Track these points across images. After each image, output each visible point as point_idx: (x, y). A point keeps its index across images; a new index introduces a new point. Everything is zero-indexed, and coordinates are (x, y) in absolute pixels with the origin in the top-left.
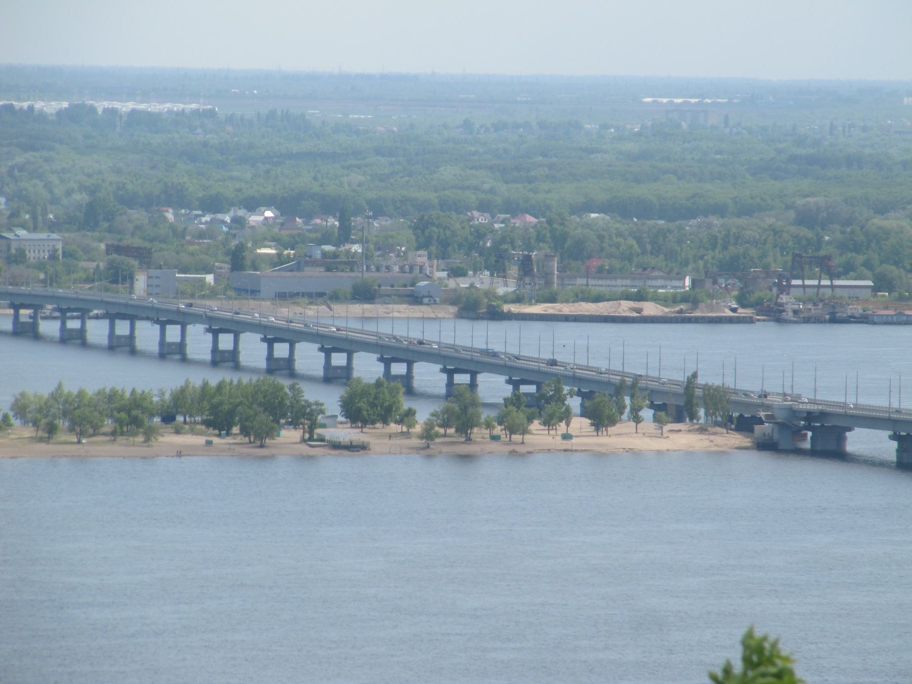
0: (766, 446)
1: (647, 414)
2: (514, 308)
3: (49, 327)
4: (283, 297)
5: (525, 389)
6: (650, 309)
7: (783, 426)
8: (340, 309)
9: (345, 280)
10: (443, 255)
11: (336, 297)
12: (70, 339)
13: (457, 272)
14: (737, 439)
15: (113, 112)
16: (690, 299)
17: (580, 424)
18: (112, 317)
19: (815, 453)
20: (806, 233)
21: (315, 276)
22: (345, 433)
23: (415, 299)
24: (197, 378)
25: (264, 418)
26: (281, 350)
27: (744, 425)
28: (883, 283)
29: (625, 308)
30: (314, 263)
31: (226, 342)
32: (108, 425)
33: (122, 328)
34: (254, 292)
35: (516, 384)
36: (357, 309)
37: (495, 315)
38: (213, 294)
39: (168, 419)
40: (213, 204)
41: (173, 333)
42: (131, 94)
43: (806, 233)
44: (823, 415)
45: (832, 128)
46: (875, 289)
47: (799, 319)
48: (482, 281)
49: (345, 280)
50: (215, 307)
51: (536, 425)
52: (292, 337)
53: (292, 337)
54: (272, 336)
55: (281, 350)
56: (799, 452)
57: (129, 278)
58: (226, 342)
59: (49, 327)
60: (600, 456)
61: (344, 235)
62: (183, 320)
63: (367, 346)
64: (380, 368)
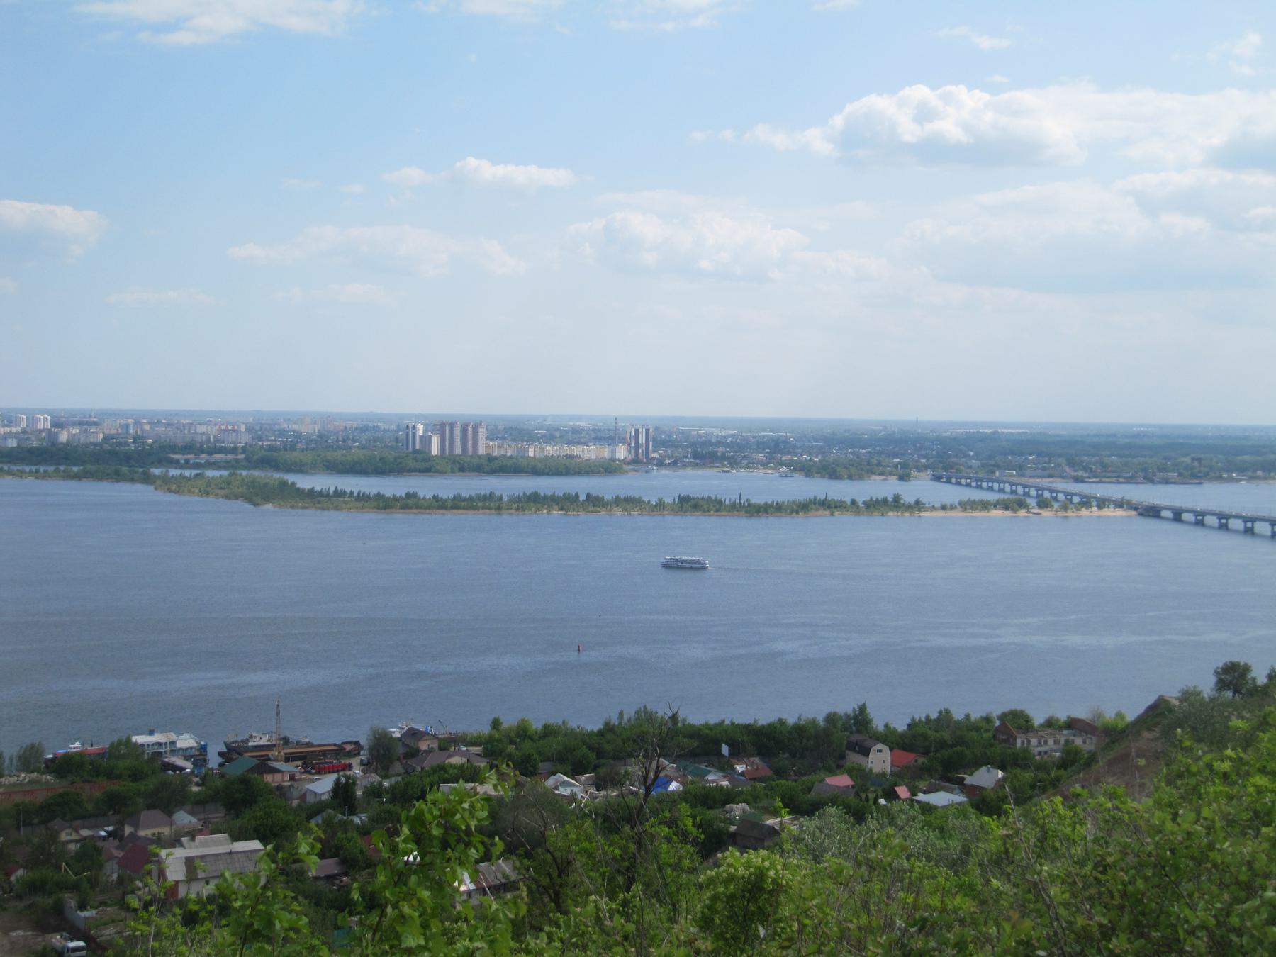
0: (1141, 514)
1: (1112, 506)
2: (1087, 480)
3: (974, 484)
4: (1031, 477)
5: (1084, 500)
6: (1121, 480)
7: (1145, 510)
8: (1044, 480)
9: (1046, 473)
10: (1073, 467)
11: (1044, 477)
12: (968, 485)
13: (1076, 471)
14: (1134, 513)
15: (1003, 432)
16: (1130, 478)
17: (1095, 509)
18: (988, 482)
19: (946, 482)
20: (1164, 461)
21: (1039, 473)
22: (1036, 511)
23: (1063, 477)
24: (1006, 497)
25: (1017, 507)
26: (1027, 490)
27: (1136, 509)
28: (1180, 475)
29: (1114, 480)
30: (1039, 469)
31: (1014, 488)
32: (979, 508)
33: (990, 484)
34: (1023, 476)
35: (1081, 499)
36: (1050, 480)
37: (1083, 481)
38: (1015, 476)
39: (995, 506)
40: (1022, 454)
41: (1002, 486)
42: (1005, 428)
43: (1164, 461)
44: (1155, 507)
45: (528, 465)
46: (1178, 476)
47: (958, 467)
48: (1080, 473)
49: (1046, 473)
50: (1012, 479)
51: (1084, 509)
52: (1029, 487)
53: (1029, 487)
54: (1025, 486)
55: (1027, 490)
56: (1149, 516)
57: (994, 472)
58: (1014, 488)
59: (974, 484)
60: (1099, 517)
61: (1050, 462)
62: (1004, 482)
63: (1032, 487)
64: (1217, 521)
